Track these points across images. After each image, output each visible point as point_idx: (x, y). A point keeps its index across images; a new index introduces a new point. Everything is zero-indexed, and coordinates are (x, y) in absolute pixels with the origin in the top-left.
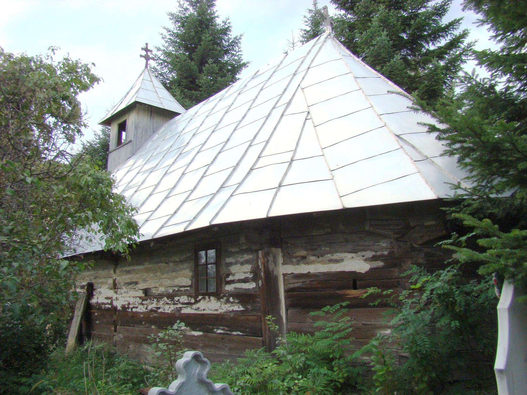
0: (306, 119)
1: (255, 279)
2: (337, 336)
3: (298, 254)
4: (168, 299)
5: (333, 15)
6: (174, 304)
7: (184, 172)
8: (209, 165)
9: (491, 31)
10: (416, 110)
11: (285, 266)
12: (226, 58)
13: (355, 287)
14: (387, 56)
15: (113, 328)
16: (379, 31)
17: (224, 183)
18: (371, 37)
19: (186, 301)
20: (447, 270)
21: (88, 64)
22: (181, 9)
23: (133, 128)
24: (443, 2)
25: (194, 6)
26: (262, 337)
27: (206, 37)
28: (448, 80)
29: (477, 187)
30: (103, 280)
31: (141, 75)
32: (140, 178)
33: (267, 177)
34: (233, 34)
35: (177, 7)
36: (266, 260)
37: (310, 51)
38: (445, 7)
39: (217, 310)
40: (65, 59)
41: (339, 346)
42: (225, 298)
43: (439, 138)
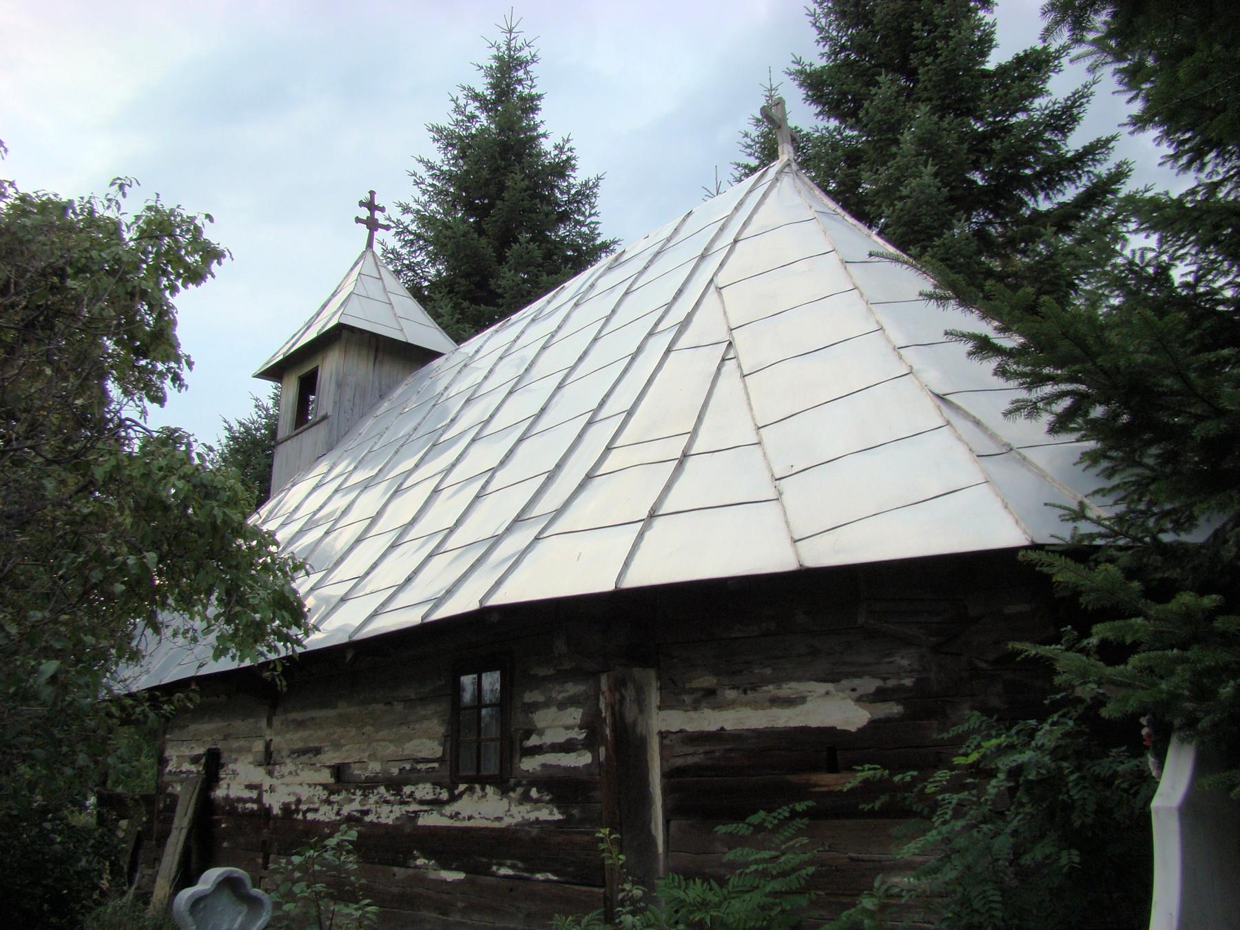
0: (723, 360)
1: (590, 744)
2: (776, 885)
3: (696, 684)
4: (388, 791)
5: (810, 130)
6: (402, 803)
7: (438, 485)
8: (494, 471)
9: (1165, 145)
10: (941, 299)
11: (664, 713)
12: (562, 232)
13: (833, 769)
14: (936, 224)
15: (260, 861)
16: (916, 165)
17: (523, 511)
18: (898, 179)
19: (430, 797)
20: (1050, 721)
21: (195, 218)
22: (460, 118)
23: (333, 385)
24: (1069, 98)
25: (491, 110)
26: (603, 886)
27: (516, 181)
28: (1082, 280)
29: (1126, 513)
30: (242, 743)
31: (356, 263)
32: (340, 502)
33: (624, 494)
34: (578, 177)
35: (451, 113)
36: (617, 696)
37: (741, 203)
38: (1075, 111)
39: (499, 819)
40: (149, 208)
41: (783, 911)
42: (520, 790)
43: (1002, 372)
